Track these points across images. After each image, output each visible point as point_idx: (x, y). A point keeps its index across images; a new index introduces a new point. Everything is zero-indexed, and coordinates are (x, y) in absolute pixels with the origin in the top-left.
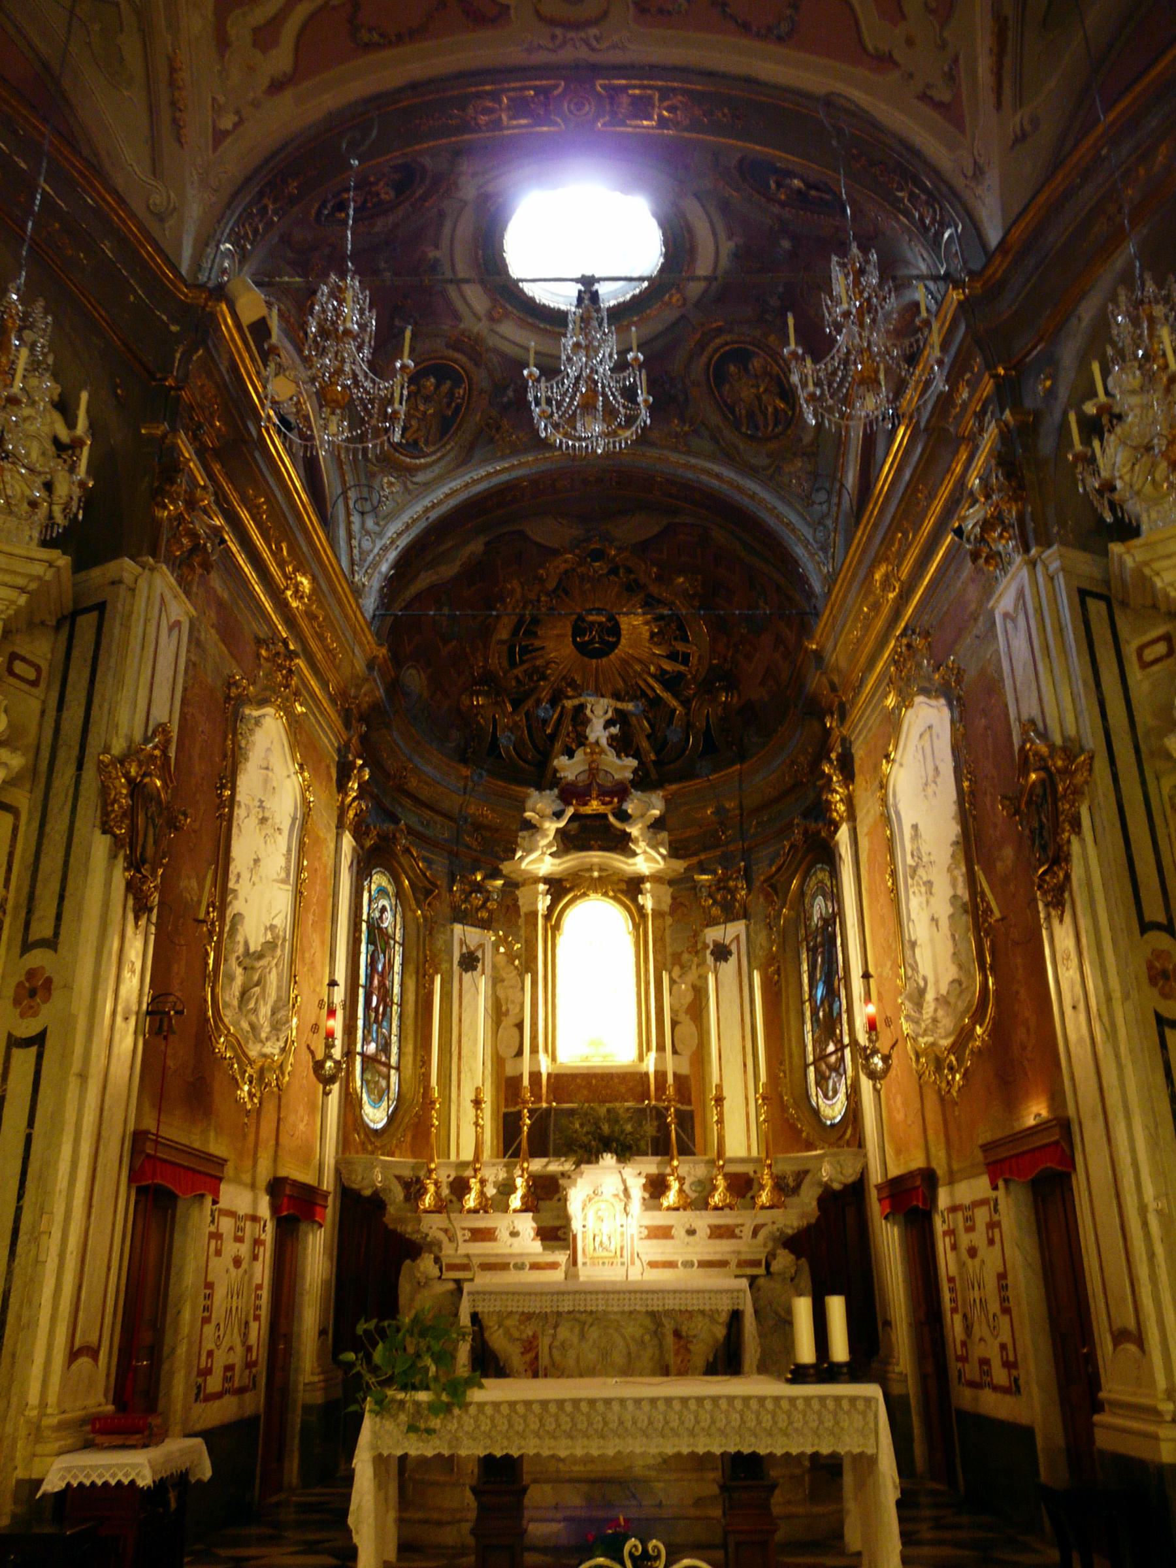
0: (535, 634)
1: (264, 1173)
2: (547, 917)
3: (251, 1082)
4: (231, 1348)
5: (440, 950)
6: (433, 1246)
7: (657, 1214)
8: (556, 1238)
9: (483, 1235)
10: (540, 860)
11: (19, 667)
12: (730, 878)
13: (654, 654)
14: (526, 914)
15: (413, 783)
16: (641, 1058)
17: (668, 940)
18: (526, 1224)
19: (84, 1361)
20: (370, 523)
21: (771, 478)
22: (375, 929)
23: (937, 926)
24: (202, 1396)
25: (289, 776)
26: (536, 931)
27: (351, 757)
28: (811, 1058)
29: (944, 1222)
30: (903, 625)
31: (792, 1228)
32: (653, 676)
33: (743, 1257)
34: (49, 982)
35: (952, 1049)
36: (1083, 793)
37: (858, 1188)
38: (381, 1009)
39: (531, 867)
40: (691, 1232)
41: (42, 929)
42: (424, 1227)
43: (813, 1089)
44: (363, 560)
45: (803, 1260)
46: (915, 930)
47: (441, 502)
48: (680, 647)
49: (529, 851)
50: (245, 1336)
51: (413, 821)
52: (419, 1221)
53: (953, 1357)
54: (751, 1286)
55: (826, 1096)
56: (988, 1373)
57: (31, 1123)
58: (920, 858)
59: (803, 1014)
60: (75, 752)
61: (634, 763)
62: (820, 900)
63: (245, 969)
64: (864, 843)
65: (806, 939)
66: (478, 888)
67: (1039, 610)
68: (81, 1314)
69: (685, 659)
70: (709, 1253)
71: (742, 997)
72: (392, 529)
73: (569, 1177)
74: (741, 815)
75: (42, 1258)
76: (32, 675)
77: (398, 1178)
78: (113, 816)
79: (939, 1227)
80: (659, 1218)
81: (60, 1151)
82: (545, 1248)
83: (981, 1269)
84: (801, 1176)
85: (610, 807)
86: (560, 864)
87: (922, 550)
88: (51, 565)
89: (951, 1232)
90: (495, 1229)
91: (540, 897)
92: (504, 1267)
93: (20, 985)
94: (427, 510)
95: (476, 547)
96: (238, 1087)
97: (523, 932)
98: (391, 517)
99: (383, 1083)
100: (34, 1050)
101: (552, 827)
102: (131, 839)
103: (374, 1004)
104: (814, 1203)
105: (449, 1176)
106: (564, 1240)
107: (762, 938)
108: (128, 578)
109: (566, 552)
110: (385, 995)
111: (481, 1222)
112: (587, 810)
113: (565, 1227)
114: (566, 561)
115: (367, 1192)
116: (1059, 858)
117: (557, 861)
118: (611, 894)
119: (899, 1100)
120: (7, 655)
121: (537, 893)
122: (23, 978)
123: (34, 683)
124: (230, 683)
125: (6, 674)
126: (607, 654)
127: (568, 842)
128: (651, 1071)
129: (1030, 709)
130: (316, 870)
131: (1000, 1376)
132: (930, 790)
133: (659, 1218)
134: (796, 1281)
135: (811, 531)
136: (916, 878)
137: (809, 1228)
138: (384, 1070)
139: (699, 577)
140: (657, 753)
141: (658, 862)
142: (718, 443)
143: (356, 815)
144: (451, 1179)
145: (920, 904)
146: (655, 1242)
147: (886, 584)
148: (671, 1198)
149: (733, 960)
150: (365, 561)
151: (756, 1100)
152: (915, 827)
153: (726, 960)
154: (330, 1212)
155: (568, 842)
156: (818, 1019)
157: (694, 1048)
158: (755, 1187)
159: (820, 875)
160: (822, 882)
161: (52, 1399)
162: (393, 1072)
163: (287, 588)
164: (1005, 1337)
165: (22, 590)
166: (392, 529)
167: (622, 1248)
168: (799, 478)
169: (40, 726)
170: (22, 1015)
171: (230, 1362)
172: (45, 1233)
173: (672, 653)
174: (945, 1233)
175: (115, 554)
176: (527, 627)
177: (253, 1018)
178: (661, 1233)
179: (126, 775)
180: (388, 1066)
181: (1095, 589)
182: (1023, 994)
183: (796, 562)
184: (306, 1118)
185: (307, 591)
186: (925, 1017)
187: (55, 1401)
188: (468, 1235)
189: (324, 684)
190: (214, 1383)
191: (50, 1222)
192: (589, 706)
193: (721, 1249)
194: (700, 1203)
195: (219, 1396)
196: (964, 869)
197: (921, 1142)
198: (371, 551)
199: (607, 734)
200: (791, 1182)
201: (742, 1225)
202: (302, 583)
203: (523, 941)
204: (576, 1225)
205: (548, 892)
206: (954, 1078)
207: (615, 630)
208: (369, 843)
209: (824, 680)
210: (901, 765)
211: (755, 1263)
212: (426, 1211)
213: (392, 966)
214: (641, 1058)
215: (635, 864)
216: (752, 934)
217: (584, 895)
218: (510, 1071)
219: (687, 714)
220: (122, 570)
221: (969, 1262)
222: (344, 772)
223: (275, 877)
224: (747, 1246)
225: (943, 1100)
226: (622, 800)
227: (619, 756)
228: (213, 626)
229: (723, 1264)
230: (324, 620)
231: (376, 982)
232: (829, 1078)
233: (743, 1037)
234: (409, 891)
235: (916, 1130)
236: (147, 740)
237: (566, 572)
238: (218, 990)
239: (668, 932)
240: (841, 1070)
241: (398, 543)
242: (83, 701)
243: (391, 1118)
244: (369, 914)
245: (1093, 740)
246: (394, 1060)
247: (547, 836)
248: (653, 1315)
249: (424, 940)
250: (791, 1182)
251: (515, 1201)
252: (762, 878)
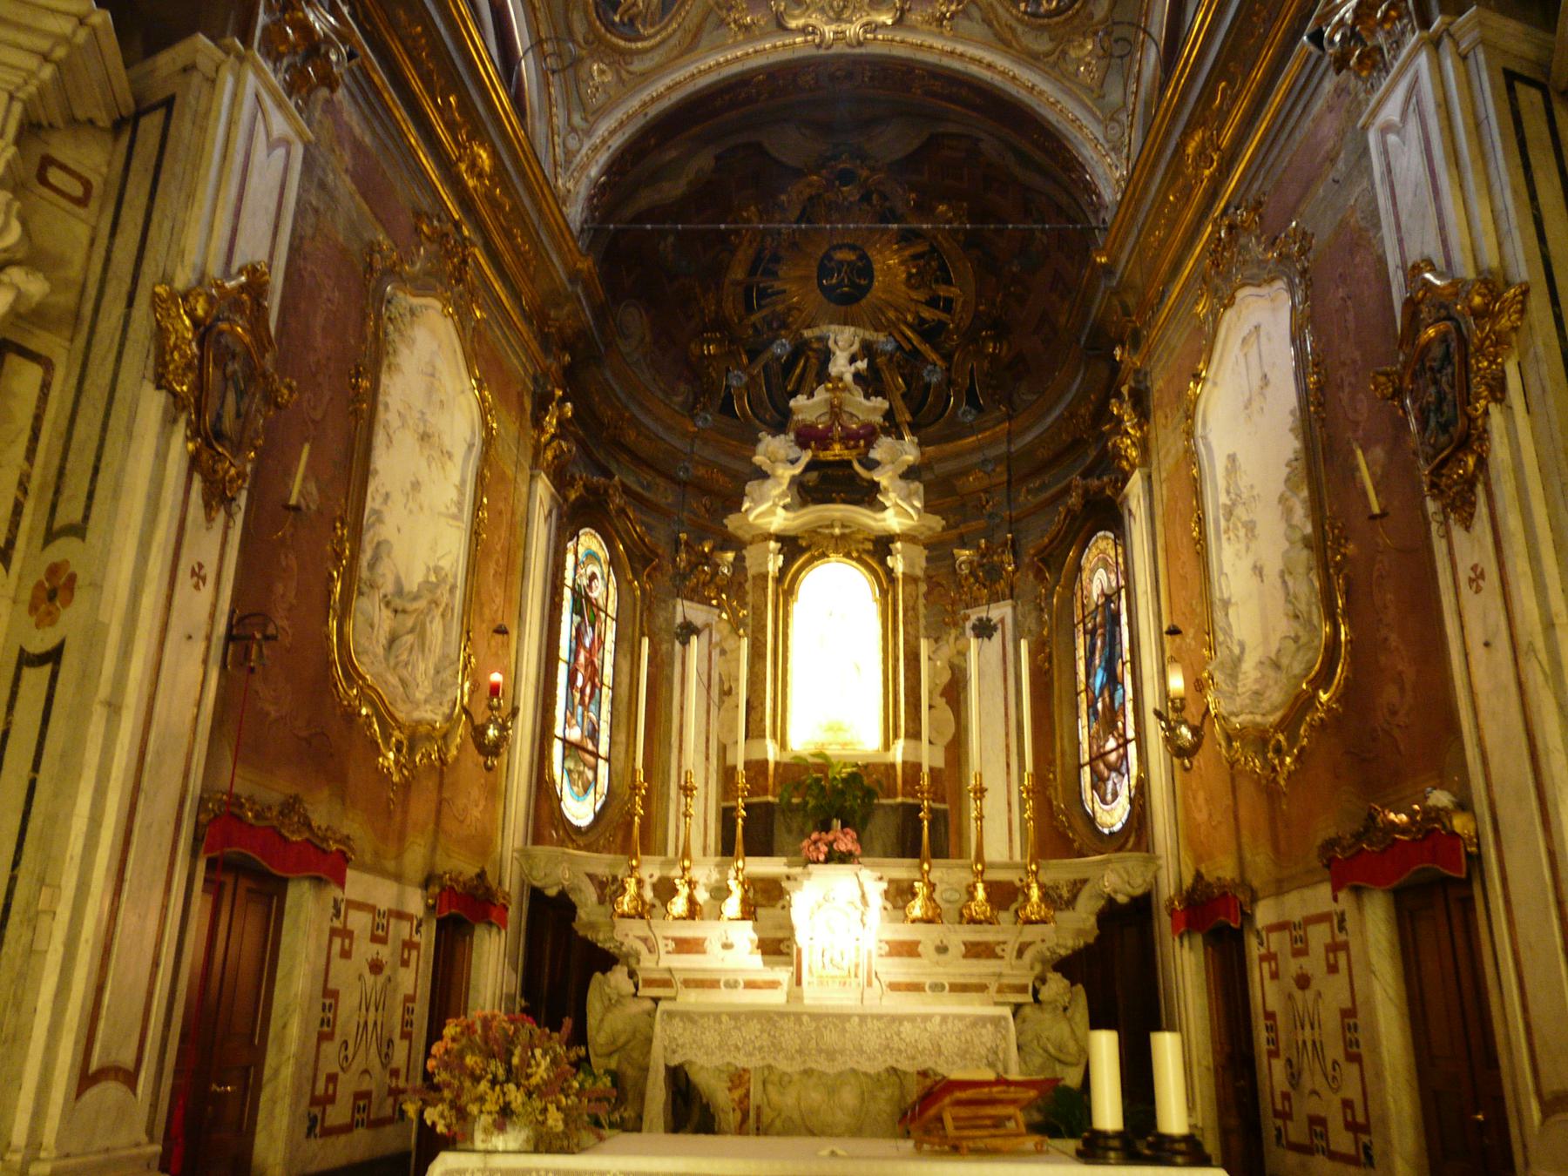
0: (775, 274)
1: (415, 857)
2: (779, 580)
3: (399, 750)
4: (366, 1071)
5: (660, 629)
7: (900, 926)
8: (779, 952)
9: (685, 946)
10: (771, 512)
11: (55, 176)
12: (995, 552)
13: (912, 300)
14: (754, 577)
15: (631, 436)
17: (922, 610)
18: (745, 934)
19: (111, 1091)
20: (577, 119)
21: (1055, 65)
22: (583, 602)
23: (1261, 575)
24: (318, 1130)
25: (463, 392)
26: (766, 596)
27: (549, 388)
28: (1085, 758)
29: (1261, 944)
30: (1222, 204)
31: (1066, 947)
32: (910, 326)
33: (1005, 981)
34: (72, 578)
35: (1280, 726)
36: (1510, 344)
37: (1142, 906)
38: (588, 690)
39: (760, 521)
40: (942, 949)
41: (70, 512)
42: (618, 936)
43: (1087, 793)
44: (568, 162)
45: (1080, 987)
46: (1228, 586)
47: (660, 96)
48: (943, 291)
49: (757, 502)
50: (386, 1058)
51: (631, 482)
52: (613, 927)
53: (1270, 1113)
54: (1014, 1015)
55: (1104, 801)
56: (1324, 1136)
57: (36, 767)
58: (1238, 495)
59: (1076, 707)
60: (126, 287)
61: (886, 405)
62: (1101, 573)
63: (396, 611)
64: (1161, 492)
65: (1083, 621)
67: (1444, 105)
68: (102, 1025)
70: (963, 975)
71: (1006, 688)
72: (603, 128)
73: (796, 879)
74: (1009, 482)
75: (38, 946)
76: (77, 190)
77: (591, 877)
78: (171, 367)
79: (1254, 949)
80: (905, 932)
81: (74, 804)
82: (765, 963)
83: (1316, 1001)
84: (1077, 886)
85: (854, 452)
86: (794, 519)
87: (1252, 101)
88: (82, 21)
89: (1269, 957)
90: (704, 940)
91: (771, 556)
92: (713, 984)
93: (39, 585)
94: (644, 105)
95: (704, 161)
96: (378, 753)
97: (749, 599)
98: (602, 112)
99: (590, 774)
100: (47, 669)
101: (786, 473)
102: (198, 401)
103: (580, 683)
104: (1093, 920)
105: (651, 876)
106: (788, 954)
108: (205, 65)
109: (811, 172)
110: (594, 673)
111: (689, 930)
112: (828, 456)
113: (789, 939)
114: (810, 185)
115: (552, 892)
116: (1471, 438)
117: (791, 515)
118: (855, 554)
119: (1201, 796)
120: (37, 160)
121: (768, 551)
122: (43, 577)
123: (82, 202)
124: (372, 248)
125: (35, 181)
126: (857, 300)
128: (899, 760)
129: (1423, 243)
130: (500, 513)
131: (1342, 1141)
132: (1255, 406)
133: (905, 932)
134: (1069, 1012)
135: (1102, 128)
136: (1233, 519)
137: (1087, 947)
138: (591, 759)
139: (965, 204)
140: (913, 415)
141: (911, 517)
142: (990, 25)
143: (555, 457)
144: (655, 879)
145: (1237, 555)
146: (897, 960)
147: (1202, 156)
148: (917, 908)
149: (997, 636)
150: (570, 162)
151: (1021, 792)
152: (1232, 458)
153: (990, 637)
154: (516, 914)
155: (807, 492)
156: (1096, 712)
157: (950, 736)
158: (1021, 898)
159: (1102, 545)
160: (1103, 552)
161: (49, 1136)
162: (601, 762)
163: (460, 159)
164: (1352, 1091)
165: (45, 58)
167: (857, 966)
168: (1088, 65)
169: (89, 258)
170: (37, 626)
171: (364, 1087)
172: (45, 912)
173: (932, 298)
174: (1262, 959)
175: (189, 31)
176: (764, 264)
177: (405, 673)
178: (907, 949)
179: (191, 314)
180: (596, 755)
181: (1526, 73)
182: (1394, 639)
183: (1083, 167)
184: (482, 803)
185: (487, 169)
186: (1240, 690)
187: (53, 1141)
188: (672, 945)
189: (516, 295)
190: (338, 1114)
191: (55, 899)
192: (832, 337)
195: (347, 1129)
196: (1305, 493)
197: (1233, 847)
198: (578, 151)
199: (852, 369)
200: (1066, 894)
201: (1004, 943)
202: (480, 157)
203: (750, 608)
204: (801, 938)
205: (780, 552)
206: (1282, 763)
207: (866, 271)
208: (573, 496)
209: (1115, 302)
210: (1215, 384)
211: (1022, 989)
212: (623, 916)
213: (602, 643)
214: (887, 747)
215: (884, 520)
216: (1020, 618)
217: (824, 555)
219: (948, 370)
220: (196, 51)
221: (1298, 994)
222: (542, 403)
223: (443, 509)
225: (1270, 791)
226: (870, 445)
227: (867, 397)
228: (347, 171)
230: (511, 210)
231: (582, 658)
232: (1108, 779)
233: (1007, 735)
234: (625, 559)
235: (1224, 833)
236: (227, 275)
237: (811, 198)
238: (349, 628)
239: (922, 601)
240: (1124, 770)
241: (610, 143)
242: (140, 221)
243: (598, 816)
244: (574, 580)
245: (1523, 268)
246: (603, 749)
247: (780, 484)
249: (642, 615)
250: (1066, 894)
251: (733, 906)
252: (1032, 552)
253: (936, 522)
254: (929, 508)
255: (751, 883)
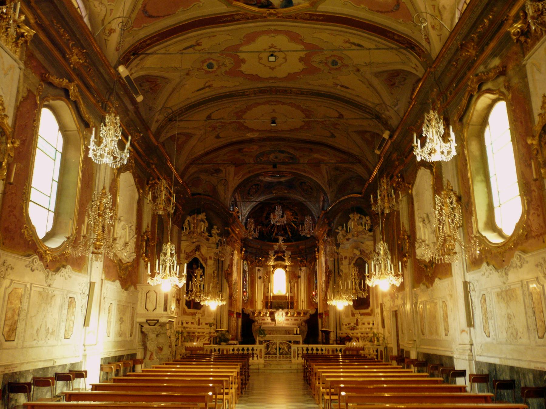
2: (272, 271)
6: (257, 321)
9: (263, 320)
16: (286, 293)
18: (269, 318)
20: (244, 208)
40: (292, 320)
48: (296, 217)
66: (260, 260)
69: (297, 219)
80: (287, 318)
82: (218, 306)
101: (273, 258)
107: (308, 271)
111: (263, 318)
127: (276, 260)
148: (289, 315)
155: (276, 260)
166: (247, 209)
193: (296, 322)
194: (293, 316)
204: (276, 319)
211: (300, 324)
218: (266, 295)
222: (242, 250)
224: (299, 322)
229: (295, 324)
248: (286, 330)
251: (268, 315)
253: (293, 264)
254: (292, 262)
255: (287, 300)
